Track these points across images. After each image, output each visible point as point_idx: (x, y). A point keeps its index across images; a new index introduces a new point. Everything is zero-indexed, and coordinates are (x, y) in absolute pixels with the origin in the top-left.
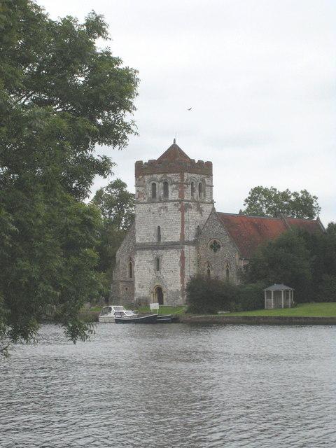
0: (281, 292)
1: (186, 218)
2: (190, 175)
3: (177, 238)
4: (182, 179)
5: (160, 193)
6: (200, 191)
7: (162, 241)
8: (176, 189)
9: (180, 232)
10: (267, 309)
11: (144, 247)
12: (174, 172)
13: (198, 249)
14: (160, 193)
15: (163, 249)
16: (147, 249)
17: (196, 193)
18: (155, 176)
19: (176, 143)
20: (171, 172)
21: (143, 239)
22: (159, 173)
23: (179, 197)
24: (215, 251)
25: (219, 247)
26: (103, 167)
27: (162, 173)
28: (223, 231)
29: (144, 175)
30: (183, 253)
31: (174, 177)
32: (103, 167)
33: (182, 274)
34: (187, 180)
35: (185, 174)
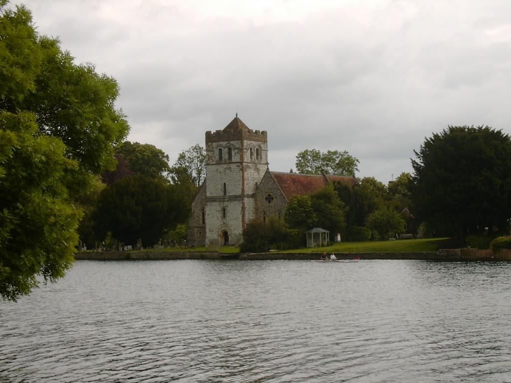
8: (238, 153)
11: (213, 199)
23: (240, 159)
29: (212, 142)
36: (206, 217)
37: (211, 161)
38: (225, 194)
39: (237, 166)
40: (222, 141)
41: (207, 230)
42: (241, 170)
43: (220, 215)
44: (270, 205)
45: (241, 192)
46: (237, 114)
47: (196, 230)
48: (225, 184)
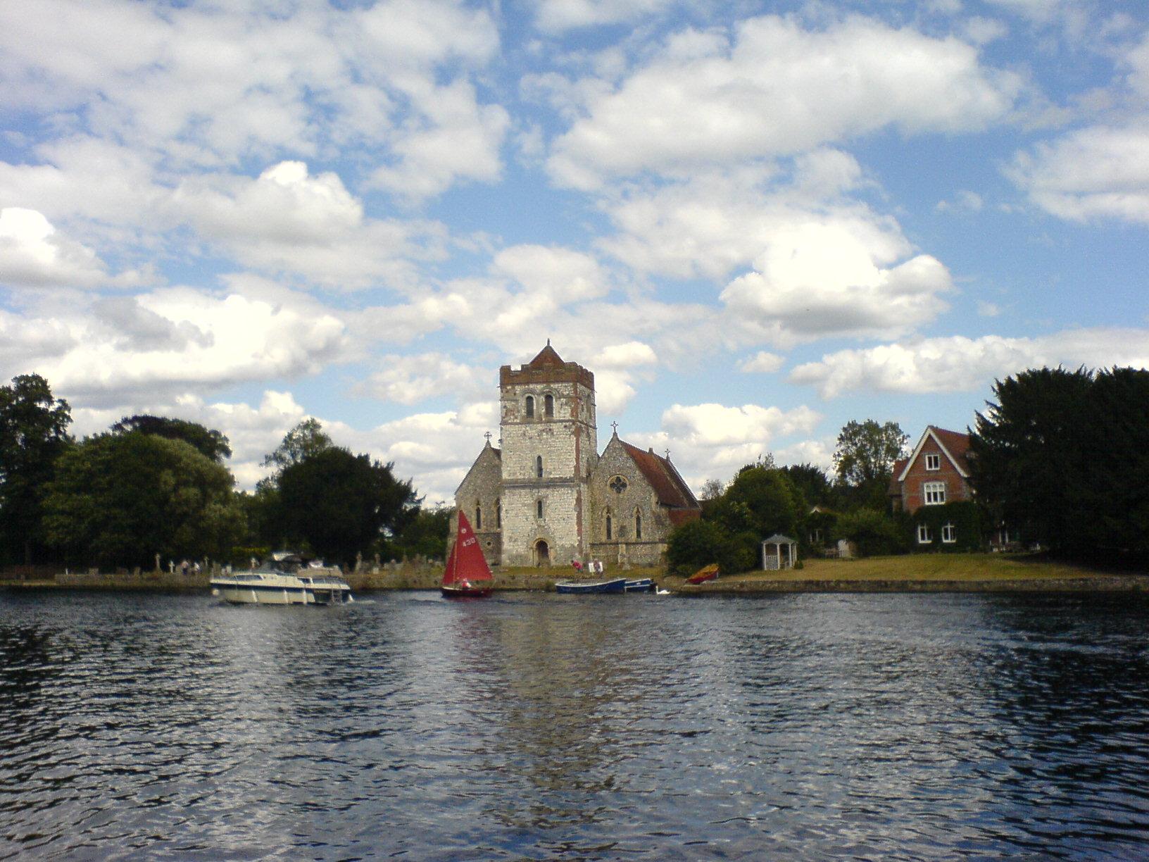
8: (566, 404)
11: (516, 485)
15: (548, 487)
16: (524, 487)
22: (537, 383)
27: (543, 382)
29: (513, 384)
36: (503, 514)
38: (540, 475)
39: (565, 426)
42: (573, 433)
43: (531, 513)
44: (621, 496)
46: (549, 341)
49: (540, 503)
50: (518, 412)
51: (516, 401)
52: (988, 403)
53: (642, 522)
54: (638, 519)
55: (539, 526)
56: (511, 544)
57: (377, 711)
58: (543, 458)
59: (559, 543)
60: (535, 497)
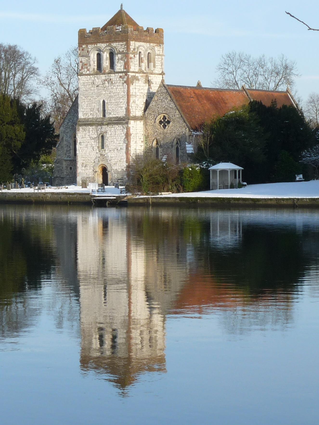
0: (228, 171)
1: (132, 91)
2: (138, 44)
3: (122, 113)
4: (128, 48)
5: (106, 63)
6: (149, 61)
7: (107, 116)
8: (121, 59)
9: (124, 106)
10: (212, 190)
11: (88, 123)
12: (120, 41)
13: (145, 124)
14: (106, 63)
15: (108, 124)
16: (91, 125)
17: (144, 65)
18: (99, 45)
19: (123, 9)
20: (116, 41)
21: (86, 114)
22: (103, 42)
23: (125, 68)
24: (164, 127)
25: (169, 122)
26: (42, 167)
27: (107, 42)
28: (172, 105)
29: (87, 44)
30: (128, 129)
31: (119, 46)
32: (42, 167)
33: (127, 152)
34: (134, 49)
35: (132, 43)
37: (86, 70)
38: (104, 115)
39: (121, 77)
40: (99, 43)
41: (79, 165)
42: (125, 82)
43: (96, 144)
44: (165, 130)
45: (125, 113)
46: (122, 5)
47: (64, 163)
48: (104, 102)
49: (103, 137)
50: (90, 65)
51: (88, 56)
52: (211, 82)
53: (180, 151)
54: (177, 149)
55: (101, 155)
56: (83, 168)
57: (50, 295)
58: (106, 101)
59: (114, 168)
60: (99, 132)
